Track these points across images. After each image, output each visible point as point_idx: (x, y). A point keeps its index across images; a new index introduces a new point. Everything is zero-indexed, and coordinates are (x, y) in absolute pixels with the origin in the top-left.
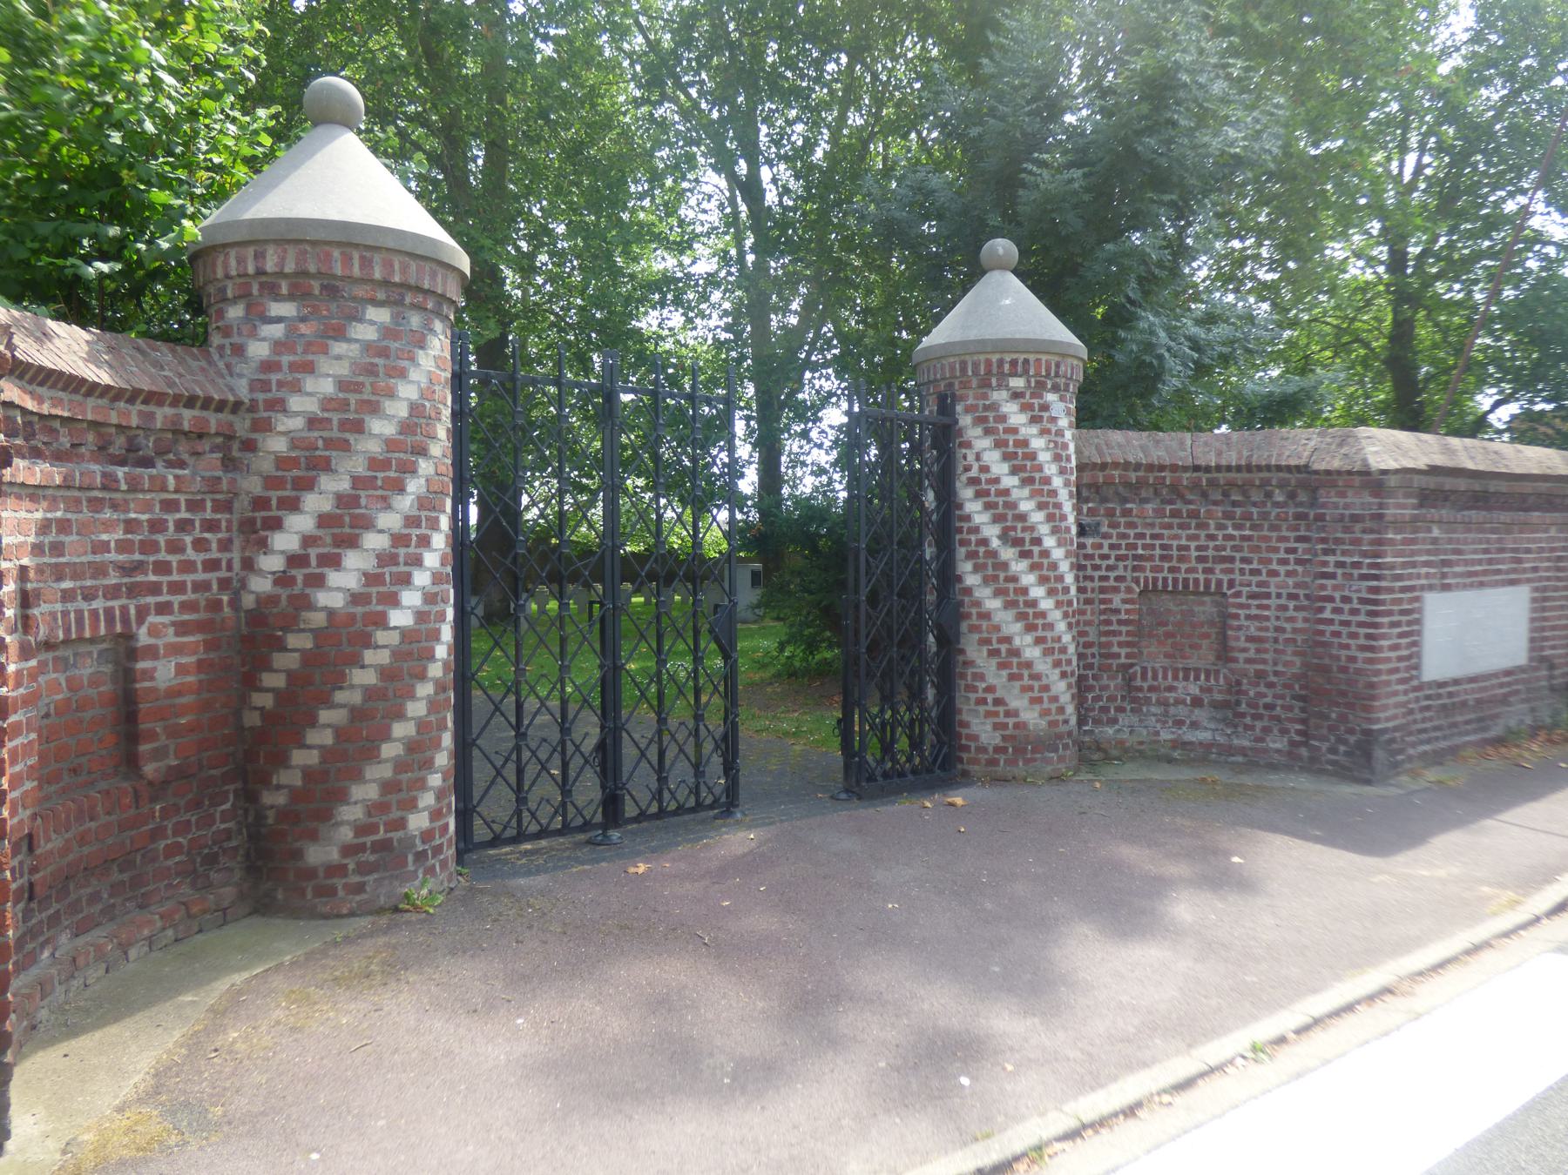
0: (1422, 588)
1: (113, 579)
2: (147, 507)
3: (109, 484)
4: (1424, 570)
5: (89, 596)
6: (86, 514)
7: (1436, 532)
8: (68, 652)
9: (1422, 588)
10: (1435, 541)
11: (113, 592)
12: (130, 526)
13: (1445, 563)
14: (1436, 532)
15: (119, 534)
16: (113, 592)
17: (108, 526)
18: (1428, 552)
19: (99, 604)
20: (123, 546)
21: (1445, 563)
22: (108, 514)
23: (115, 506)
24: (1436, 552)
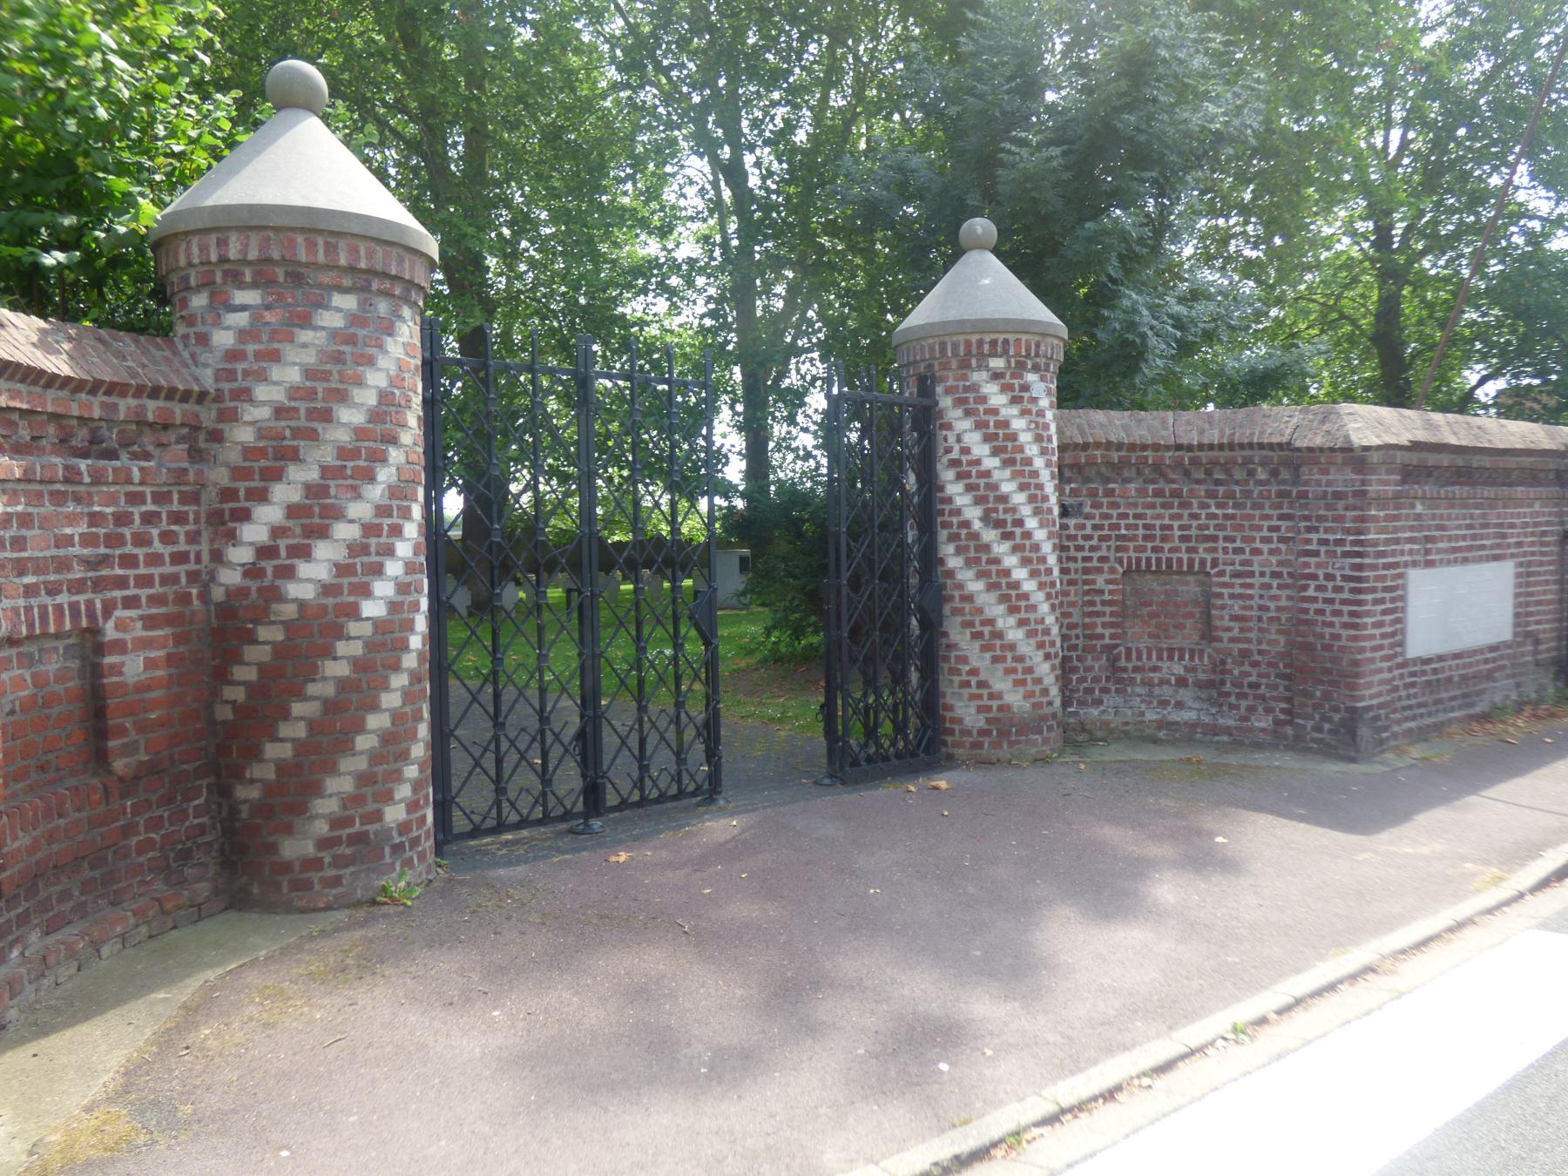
0: (1406, 565)
1: (77, 573)
2: (111, 499)
3: (72, 476)
4: (1407, 547)
5: (53, 591)
6: (48, 508)
7: (1419, 508)
8: (31, 648)
9: (1406, 565)
10: (1418, 517)
11: (77, 587)
12: (95, 519)
13: (1428, 539)
14: (1419, 508)
15: (83, 528)
16: (77, 587)
17: (71, 519)
18: (1412, 529)
19: (63, 599)
20: (87, 540)
21: (1428, 539)
22: (71, 507)
23: (78, 499)
24: (1421, 528)
